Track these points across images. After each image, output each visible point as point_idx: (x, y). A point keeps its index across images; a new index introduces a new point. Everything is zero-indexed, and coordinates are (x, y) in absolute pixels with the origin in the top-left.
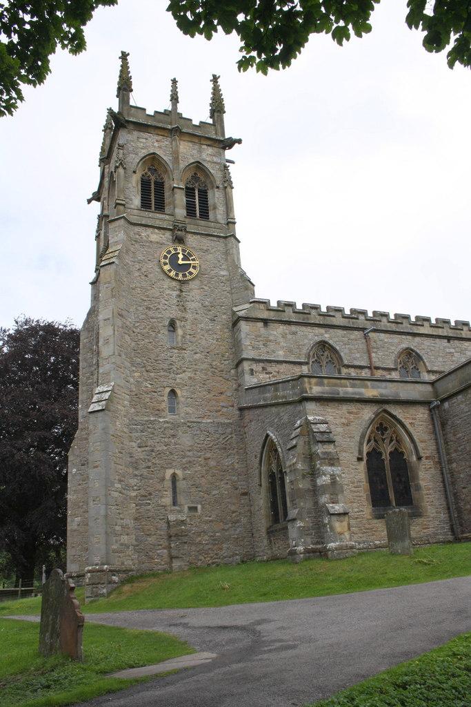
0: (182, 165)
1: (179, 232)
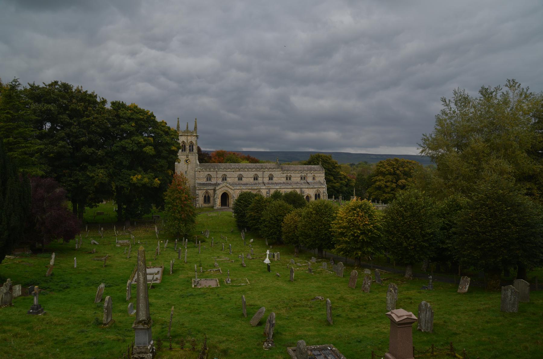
0: (189, 142)
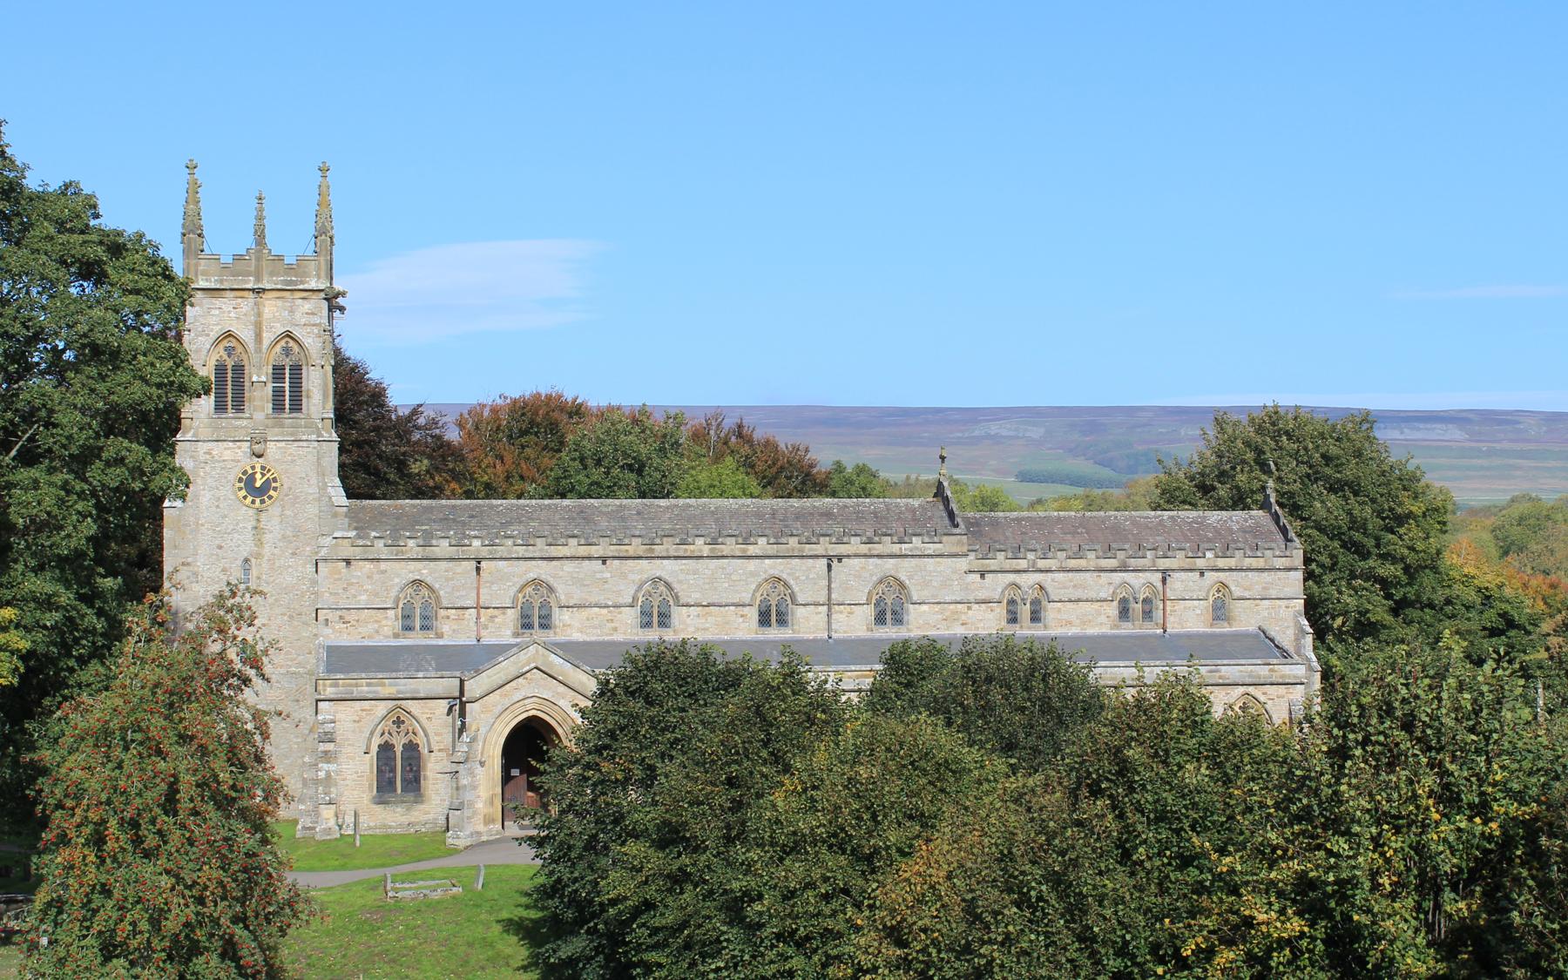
1: (257, 446)
